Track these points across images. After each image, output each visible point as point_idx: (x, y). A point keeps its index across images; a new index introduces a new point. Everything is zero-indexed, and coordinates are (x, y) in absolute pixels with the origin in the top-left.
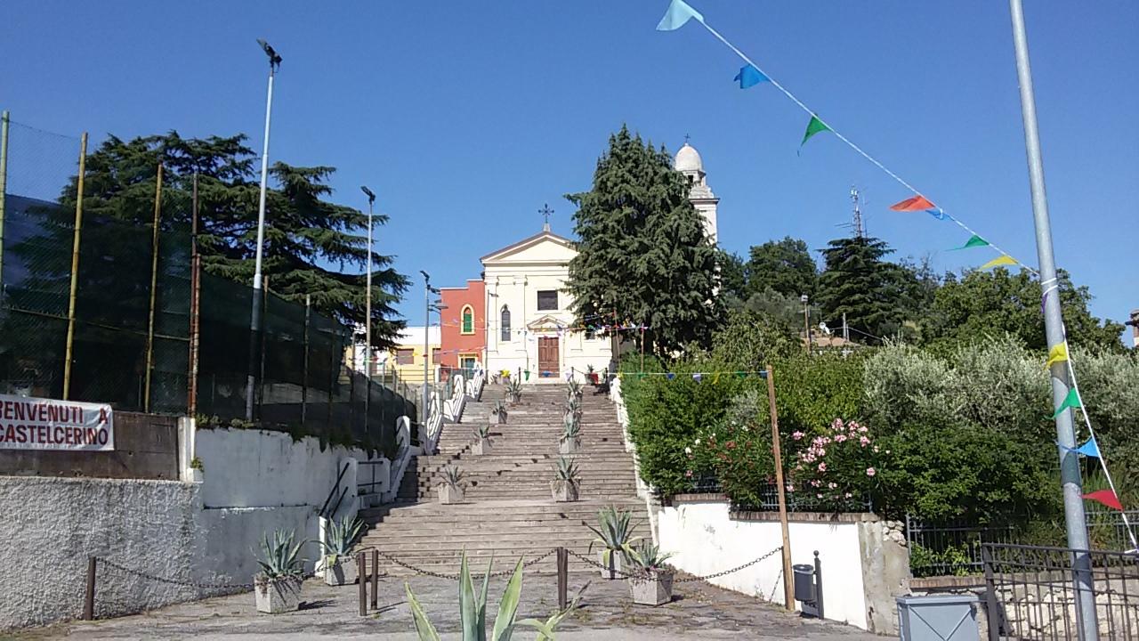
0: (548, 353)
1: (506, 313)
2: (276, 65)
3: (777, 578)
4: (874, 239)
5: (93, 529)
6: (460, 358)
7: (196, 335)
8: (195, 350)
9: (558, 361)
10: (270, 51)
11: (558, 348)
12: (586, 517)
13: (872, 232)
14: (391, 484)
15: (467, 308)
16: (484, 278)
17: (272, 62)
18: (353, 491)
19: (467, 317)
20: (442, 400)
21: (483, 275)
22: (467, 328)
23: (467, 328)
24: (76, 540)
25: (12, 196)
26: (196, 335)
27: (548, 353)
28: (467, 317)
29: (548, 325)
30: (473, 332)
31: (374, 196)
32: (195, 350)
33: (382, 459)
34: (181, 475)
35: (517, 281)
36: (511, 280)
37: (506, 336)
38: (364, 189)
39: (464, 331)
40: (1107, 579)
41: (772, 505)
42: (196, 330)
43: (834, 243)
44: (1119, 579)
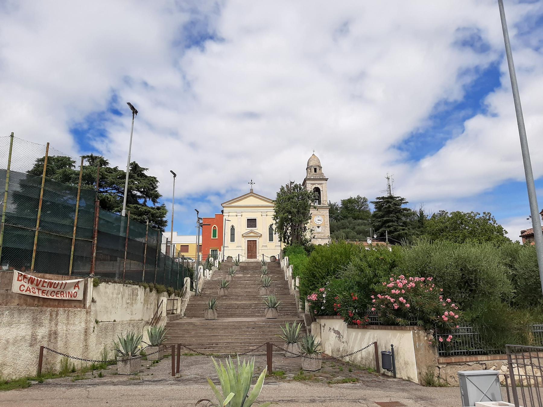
0: (252, 248)
1: (233, 229)
2: (135, 114)
3: (126, 320)
4: (398, 197)
5: (42, 332)
6: (210, 250)
7: (96, 238)
8: (95, 245)
9: (256, 251)
10: (132, 108)
11: (256, 245)
12: (371, 340)
13: (397, 193)
14: (181, 310)
15: (215, 227)
16: (223, 213)
17: (133, 113)
18: (164, 314)
19: (215, 231)
20: (204, 270)
21: (222, 211)
22: (214, 235)
23: (214, 235)
24: (34, 337)
25: (12, 171)
26: (96, 238)
27: (252, 248)
28: (215, 231)
29: (252, 234)
30: (217, 238)
31: (176, 175)
32: (95, 245)
33: (177, 298)
34: (85, 306)
35: (268, 213)
36: (235, 214)
37: (233, 240)
38: (171, 171)
39: (213, 237)
40: (524, 359)
41: (374, 322)
42: (96, 236)
43: (378, 198)
44: (528, 358)
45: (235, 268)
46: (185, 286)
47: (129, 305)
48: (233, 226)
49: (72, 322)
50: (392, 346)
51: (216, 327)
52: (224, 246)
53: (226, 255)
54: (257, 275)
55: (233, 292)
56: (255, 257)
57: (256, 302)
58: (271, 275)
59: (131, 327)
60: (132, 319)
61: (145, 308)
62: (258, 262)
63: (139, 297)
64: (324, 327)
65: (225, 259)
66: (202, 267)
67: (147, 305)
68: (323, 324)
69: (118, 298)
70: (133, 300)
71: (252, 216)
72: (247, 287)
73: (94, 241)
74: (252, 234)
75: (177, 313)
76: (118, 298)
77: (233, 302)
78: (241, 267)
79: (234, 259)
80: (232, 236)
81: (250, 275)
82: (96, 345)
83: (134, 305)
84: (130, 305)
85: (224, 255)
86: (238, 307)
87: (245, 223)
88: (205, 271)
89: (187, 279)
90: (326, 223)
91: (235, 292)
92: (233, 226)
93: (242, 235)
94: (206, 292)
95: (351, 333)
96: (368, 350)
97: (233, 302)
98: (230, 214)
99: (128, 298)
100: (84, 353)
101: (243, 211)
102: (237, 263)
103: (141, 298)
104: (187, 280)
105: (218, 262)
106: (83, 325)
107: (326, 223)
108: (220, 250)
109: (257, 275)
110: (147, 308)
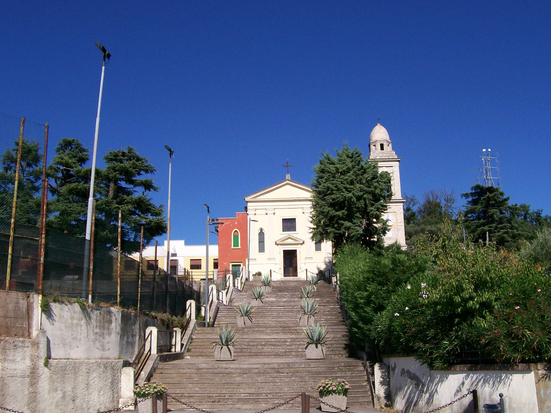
1: (261, 234)
6: (231, 264)
15: (236, 231)
16: (247, 211)
19: (236, 237)
20: (218, 291)
22: (236, 244)
23: (236, 244)
28: (236, 237)
30: (240, 247)
37: (262, 249)
46: (188, 312)
47: (98, 336)
48: (261, 230)
49: (11, 358)
50: (501, 395)
53: (253, 271)
54: (296, 299)
56: (295, 274)
57: (293, 336)
59: (103, 367)
61: (124, 342)
63: (113, 325)
65: (251, 278)
66: (214, 287)
67: (128, 338)
69: (81, 326)
71: (299, 224)
72: (281, 314)
73: (42, 239)
76: (81, 326)
77: (258, 336)
78: (274, 287)
81: (285, 299)
82: (49, 392)
85: (249, 272)
86: (267, 343)
87: (280, 225)
88: (221, 293)
89: (191, 303)
90: (399, 224)
92: (261, 230)
94: (221, 323)
96: (461, 403)
97: (258, 336)
98: (258, 212)
99: (96, 326)
100: (30, 403)
102: (267, 283)
103: (116, 326)
104: (191, 304)
106: (28, 362)
107: (399, 224)
108: (245, 265)
110: (127, 342)
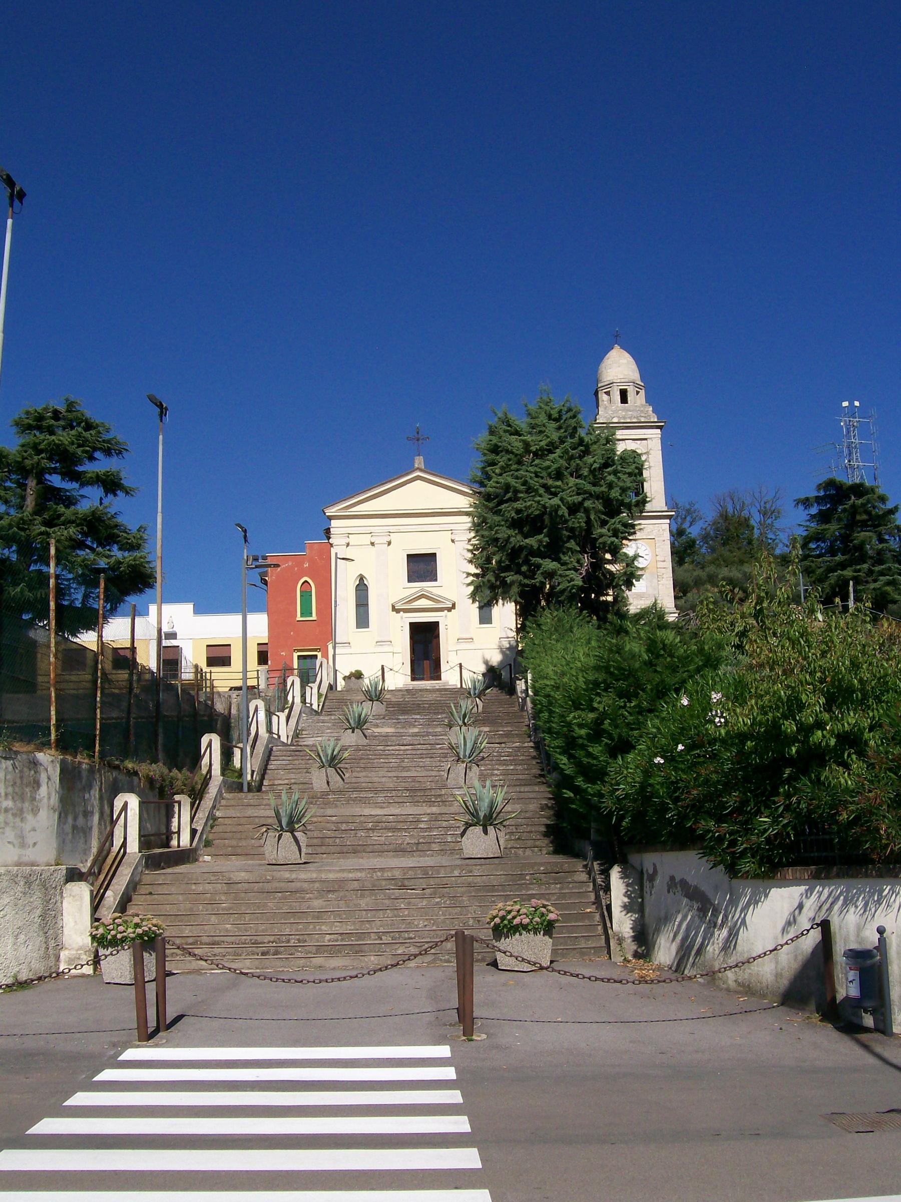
1: (362, 588)
6: (295, 655)
15: (306, 582)
16: (329, 538)
19: (306, 595)
20: (269, 714)
22: (306, 611)
23: (306, 611)
28: (306, 595)
29: (423, 603)
30: (314, 617)
36: (367, 539)
37: (362, 621)
39: (302, 615)
45: (367, 709)
46: (205, 761)
47: (10, 816)
48: (362, 578)
51: (299, 884)
52: (335, 643)
54: (439, 729)
55: (362, 780)
57: (434, 810)
58: (487, 729)
59: (22, 883)
60: (25, 859)
61: (68, 828)
62: (446, 690)
63: (43, 791)
64: (652, 878)
66: (261, 704)
67: (75, 819)
68: (648, 868)
70: (23, 801)
71: (421, 547)
74: (423, 603)
75: (181, 844)
77: (358, 810)
78: (389, 704)
79: (367, 681)
80: (362, 609)
83: (29, 817)
84: (14, 815)
85: (335, 671)
86: (378, 825)
88: (275, 719)
90: (660, 565)
91: (367, 780)
92: (362, 578)
93: (393, 607)
94: (276, 782)
95: (744, 889)
97: (358, 810)
98: (353, 540)
99: (6, 795)
101: (392, 529)
102: (375, 695)
104: (210, 743)
105: (315, 691)
107: (660, 565)
108: (325, 656)
109: (439, 729)
110: (74, 827)
